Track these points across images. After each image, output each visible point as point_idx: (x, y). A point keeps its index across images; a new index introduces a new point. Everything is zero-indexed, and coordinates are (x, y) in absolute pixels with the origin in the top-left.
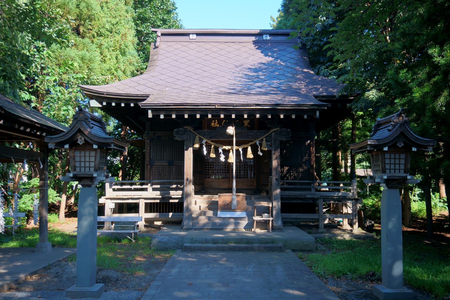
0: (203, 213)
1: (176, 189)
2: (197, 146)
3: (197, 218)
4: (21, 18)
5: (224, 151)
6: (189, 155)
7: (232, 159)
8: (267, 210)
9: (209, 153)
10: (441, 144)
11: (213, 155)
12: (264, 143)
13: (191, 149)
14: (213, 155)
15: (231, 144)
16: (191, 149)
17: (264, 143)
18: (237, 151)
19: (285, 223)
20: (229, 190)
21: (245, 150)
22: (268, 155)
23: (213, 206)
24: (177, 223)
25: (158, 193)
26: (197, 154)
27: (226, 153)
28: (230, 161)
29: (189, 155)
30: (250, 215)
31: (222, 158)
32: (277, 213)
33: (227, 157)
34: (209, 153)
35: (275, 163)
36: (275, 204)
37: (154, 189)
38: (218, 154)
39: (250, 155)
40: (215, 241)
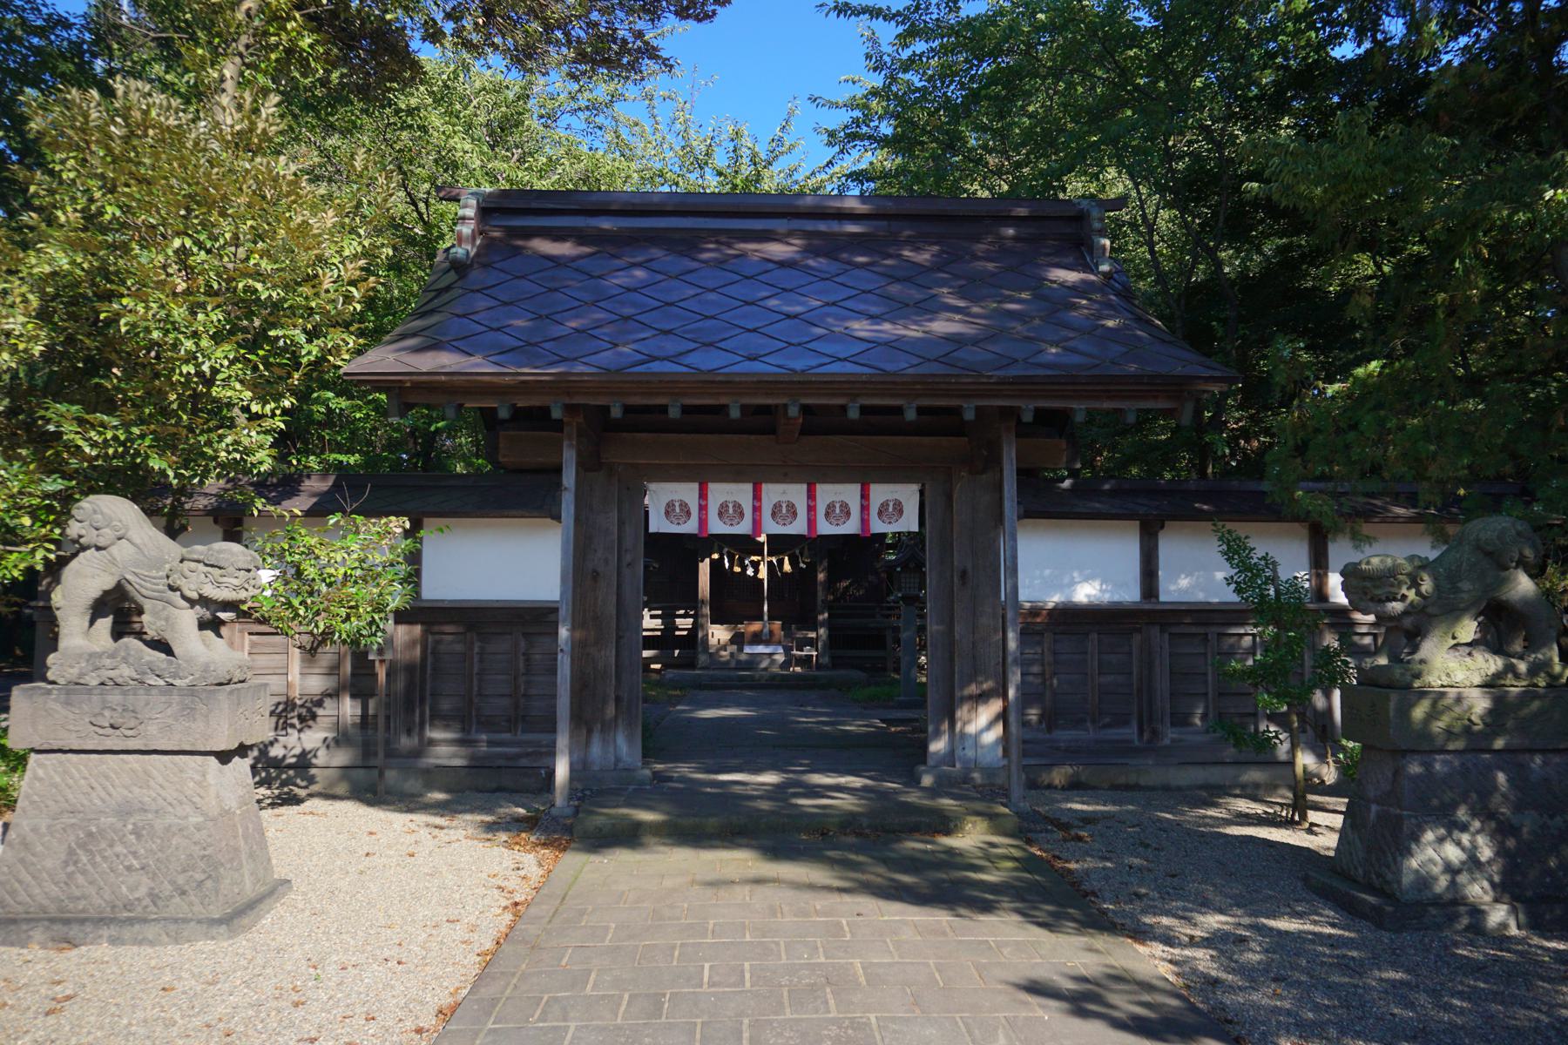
0: (724, 648)
1: (685, 616)
2: (716, 556)
3: (1120, 173)
4: (979, 788)
5: (752, 562)
6: (704, 568)
7: (763, 573)
8: (812, 643)
9: (731, 566)
10: (650, 622)
11: (737, 569)
12: (806, 552)
13: (707, 560)
14: (737, 569)
15: (761, 554)
16: (707, 560)
17: (806, 552)
18: (770, 563)
19: (836, 663)
20: (760, 618)
21: (781, 562)
22: (812, 569)
23: (738, 640)
24: (691, 664)
25: (659, 621)
26: (716, 567)
27: (756, 565)
28: (760, 576)
29: (704, 568)
30: (787, 650)
31: (750, 572)
32: (824, 645)
33: (757, 571)
34: (731, 566)
35: (821, 576)
36: (822, 631)
37: (652, 617)
38: (744, 568)
39: (787, 567)
40: (742, 678)
